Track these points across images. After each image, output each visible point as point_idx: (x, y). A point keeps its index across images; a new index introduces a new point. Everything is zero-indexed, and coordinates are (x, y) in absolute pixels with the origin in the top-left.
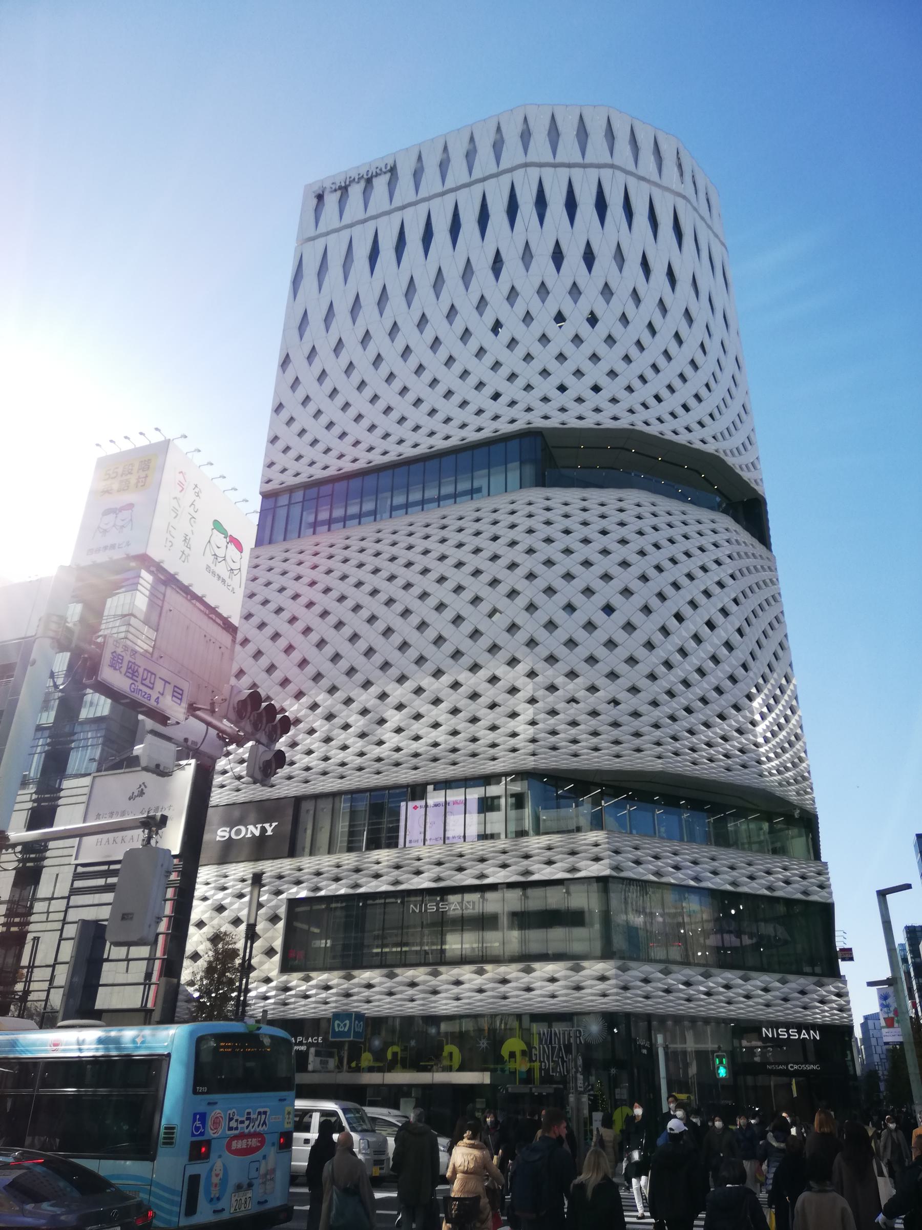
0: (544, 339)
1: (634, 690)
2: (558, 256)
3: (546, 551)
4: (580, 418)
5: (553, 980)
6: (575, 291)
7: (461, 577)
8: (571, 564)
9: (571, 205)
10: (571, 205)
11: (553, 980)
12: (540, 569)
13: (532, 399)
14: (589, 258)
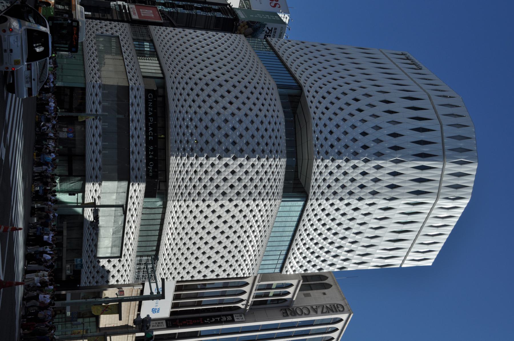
2: (395, 135)
6: (364, 134)
12: (255, 126)
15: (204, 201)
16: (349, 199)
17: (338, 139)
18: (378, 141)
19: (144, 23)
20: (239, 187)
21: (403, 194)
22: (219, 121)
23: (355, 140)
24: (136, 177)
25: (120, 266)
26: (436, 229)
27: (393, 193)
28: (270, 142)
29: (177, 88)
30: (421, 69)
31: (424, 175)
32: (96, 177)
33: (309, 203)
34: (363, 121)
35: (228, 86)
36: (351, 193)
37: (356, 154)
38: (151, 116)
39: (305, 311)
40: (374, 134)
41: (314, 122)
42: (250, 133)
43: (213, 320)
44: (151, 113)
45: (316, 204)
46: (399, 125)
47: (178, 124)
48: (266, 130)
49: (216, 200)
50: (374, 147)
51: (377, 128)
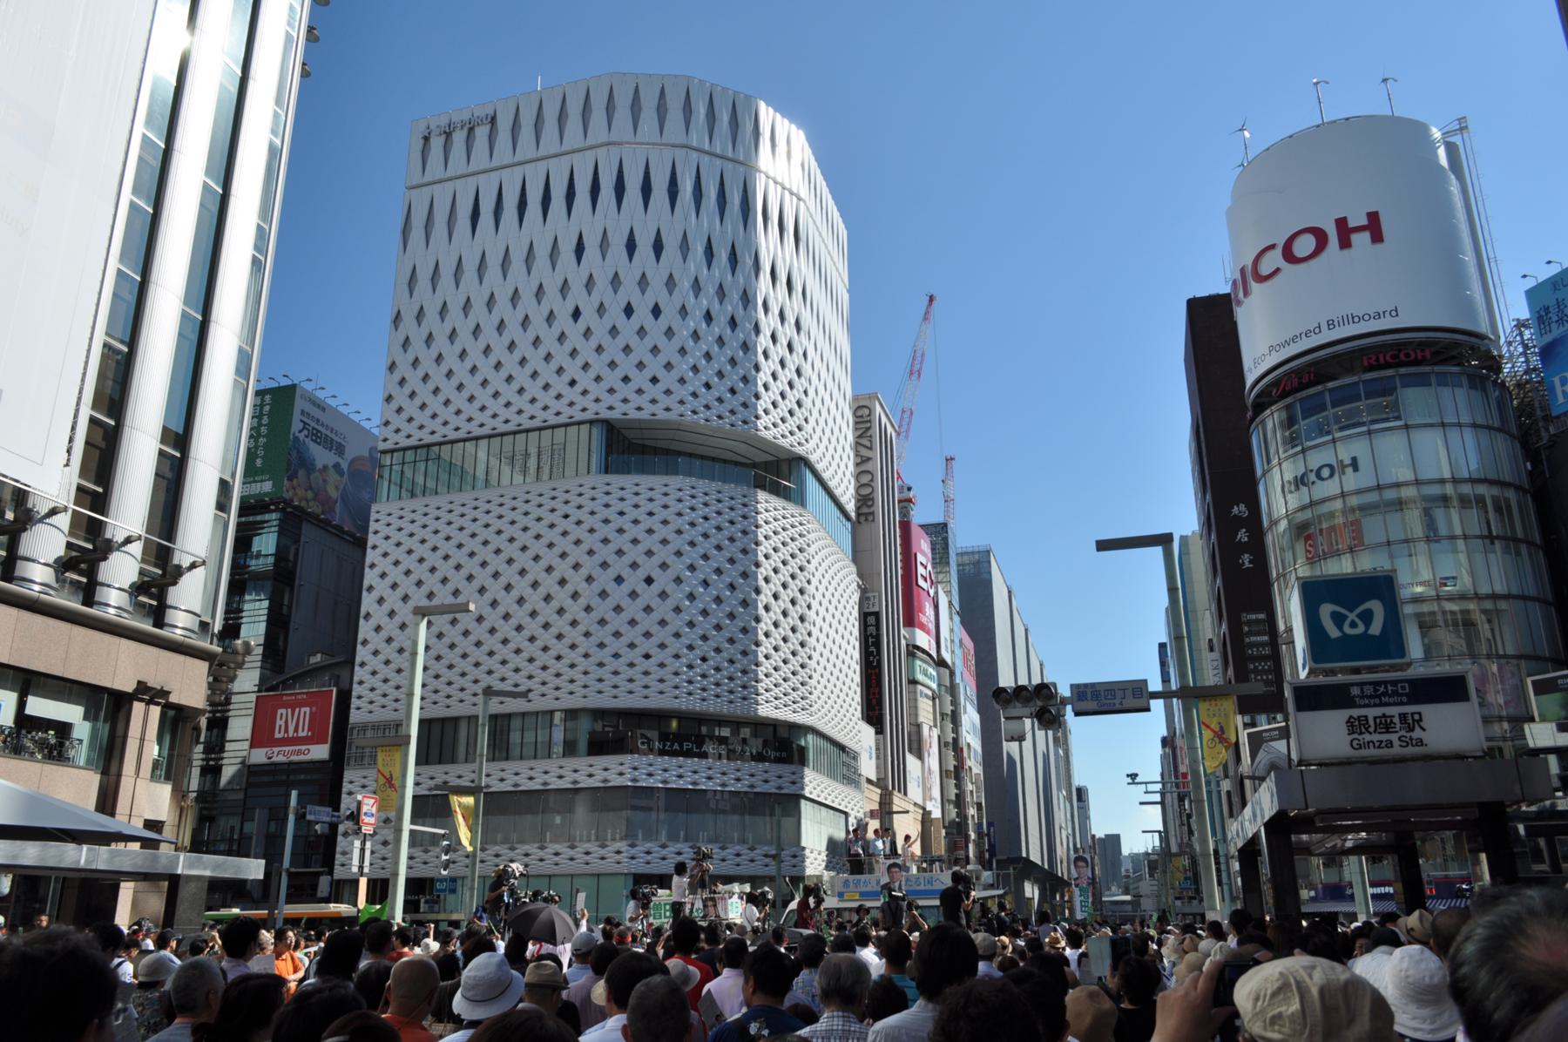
0: (599, 349)
1: (601, 645)
2: (631, 246)
3: (648, 522)
4: (611, 408)
5: (618, 852)
6: (629, 311)
7: (412, 543)
8: (637, 531)
11: (618, 852)
12: (671, 537)
13: (671, 401)
14: (658, 247)
18: (643, 282)
22: (603, 609)
23: (642, 332)
24: (794, 783)
29: (385, 695)
30: (493, 120)
32: (794, 856)
34: (601, 310)
37: (746, 347)
38: (681, 746)
39: (865, 479)
40: (629, 291)
41: (662, 415)
42: (598, 547)
43: (872, 649)
44: (676, 746)
46: (609, 234)
47: (443, 701)
48: (651, 514)
50: (733, 305)
51: (616, 281)
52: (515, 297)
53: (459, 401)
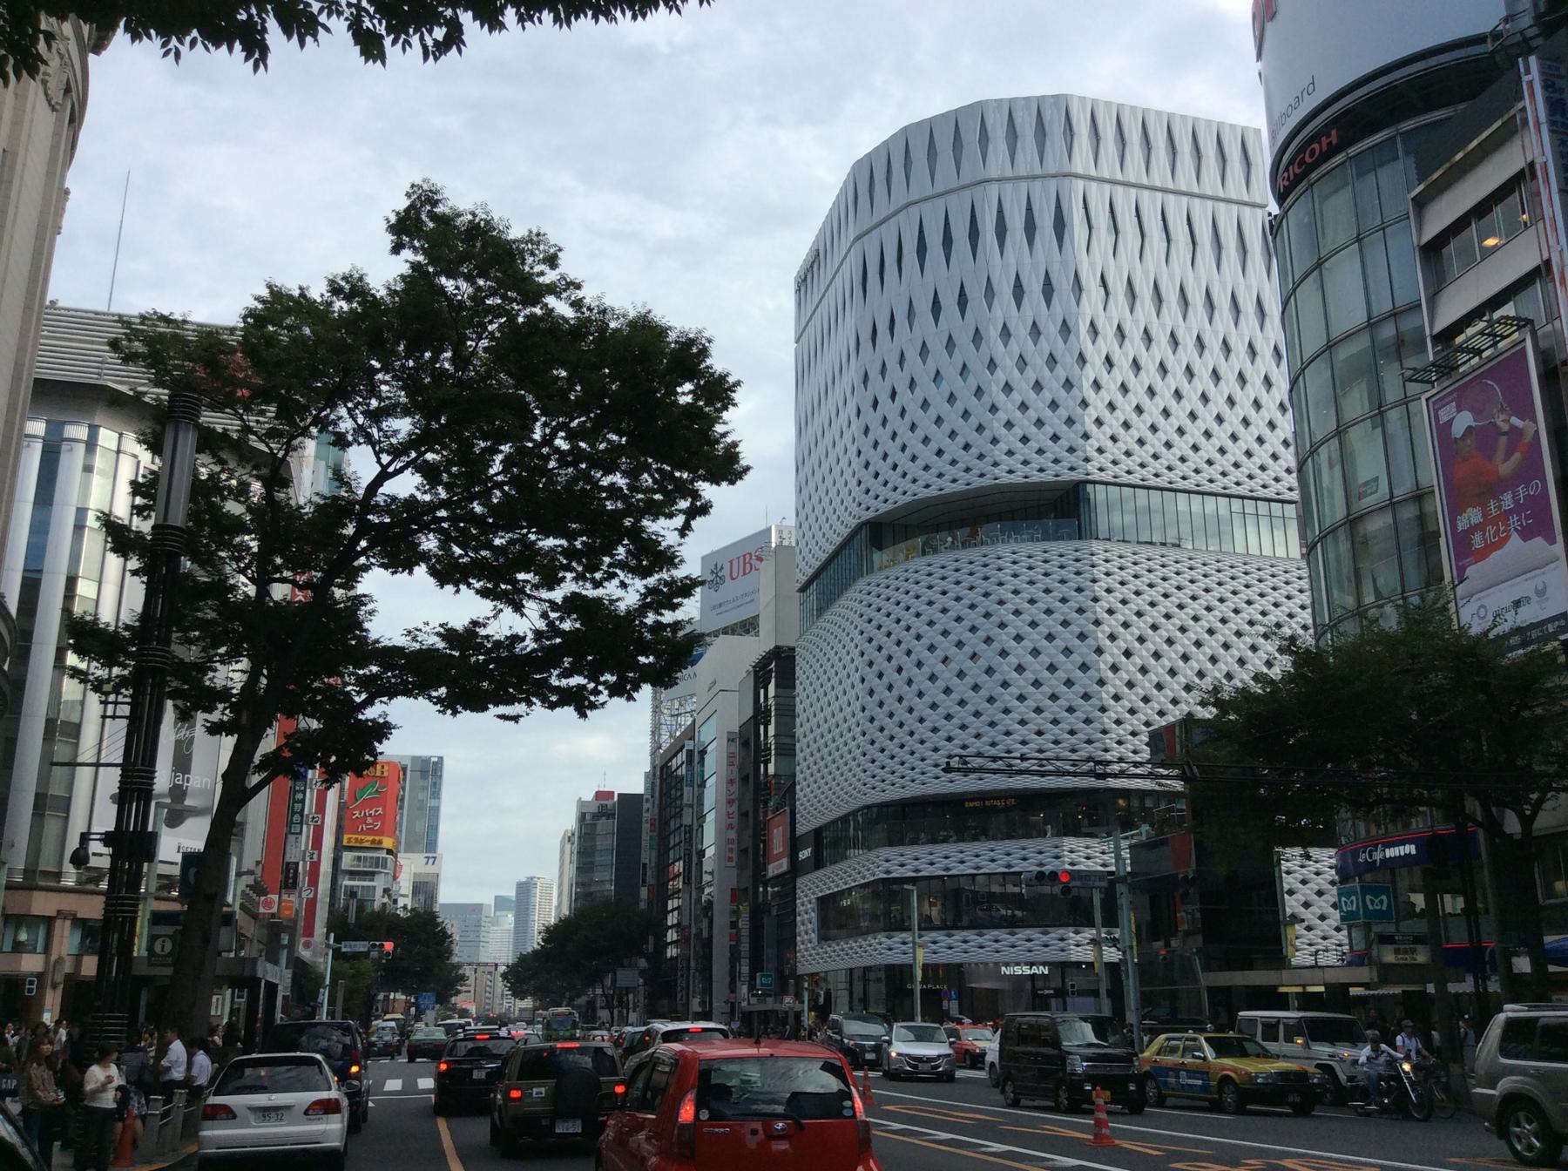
2: (1019, 291)
9: (1030, 227)
10: (1030, 227)
14: (1048, 290)
15: (1101, 683)
16: (1081, 388)
17: (947, 691)
19: (795, 844)
20: (1066, 637)
21: (1064, 263)
25: (1305, 889)
26: (1173, 245)
27: (1063, 285)
28: (1059, 574)
31: (1016, 223)
33: (1097, 476)
35: (870, 649)
36: (1068, 385)
45: (1099, 460)
49: (1099, 651)
52: (950, 344)
53: (953, 449)
